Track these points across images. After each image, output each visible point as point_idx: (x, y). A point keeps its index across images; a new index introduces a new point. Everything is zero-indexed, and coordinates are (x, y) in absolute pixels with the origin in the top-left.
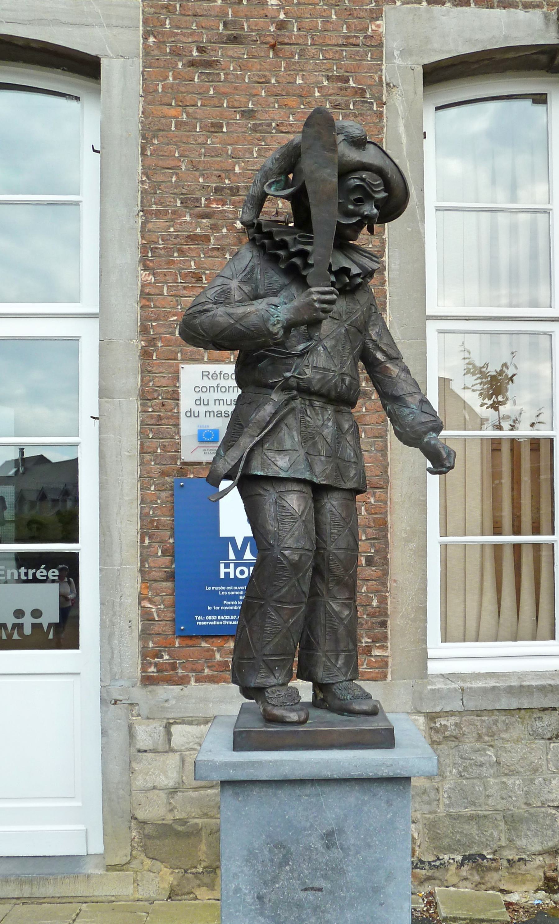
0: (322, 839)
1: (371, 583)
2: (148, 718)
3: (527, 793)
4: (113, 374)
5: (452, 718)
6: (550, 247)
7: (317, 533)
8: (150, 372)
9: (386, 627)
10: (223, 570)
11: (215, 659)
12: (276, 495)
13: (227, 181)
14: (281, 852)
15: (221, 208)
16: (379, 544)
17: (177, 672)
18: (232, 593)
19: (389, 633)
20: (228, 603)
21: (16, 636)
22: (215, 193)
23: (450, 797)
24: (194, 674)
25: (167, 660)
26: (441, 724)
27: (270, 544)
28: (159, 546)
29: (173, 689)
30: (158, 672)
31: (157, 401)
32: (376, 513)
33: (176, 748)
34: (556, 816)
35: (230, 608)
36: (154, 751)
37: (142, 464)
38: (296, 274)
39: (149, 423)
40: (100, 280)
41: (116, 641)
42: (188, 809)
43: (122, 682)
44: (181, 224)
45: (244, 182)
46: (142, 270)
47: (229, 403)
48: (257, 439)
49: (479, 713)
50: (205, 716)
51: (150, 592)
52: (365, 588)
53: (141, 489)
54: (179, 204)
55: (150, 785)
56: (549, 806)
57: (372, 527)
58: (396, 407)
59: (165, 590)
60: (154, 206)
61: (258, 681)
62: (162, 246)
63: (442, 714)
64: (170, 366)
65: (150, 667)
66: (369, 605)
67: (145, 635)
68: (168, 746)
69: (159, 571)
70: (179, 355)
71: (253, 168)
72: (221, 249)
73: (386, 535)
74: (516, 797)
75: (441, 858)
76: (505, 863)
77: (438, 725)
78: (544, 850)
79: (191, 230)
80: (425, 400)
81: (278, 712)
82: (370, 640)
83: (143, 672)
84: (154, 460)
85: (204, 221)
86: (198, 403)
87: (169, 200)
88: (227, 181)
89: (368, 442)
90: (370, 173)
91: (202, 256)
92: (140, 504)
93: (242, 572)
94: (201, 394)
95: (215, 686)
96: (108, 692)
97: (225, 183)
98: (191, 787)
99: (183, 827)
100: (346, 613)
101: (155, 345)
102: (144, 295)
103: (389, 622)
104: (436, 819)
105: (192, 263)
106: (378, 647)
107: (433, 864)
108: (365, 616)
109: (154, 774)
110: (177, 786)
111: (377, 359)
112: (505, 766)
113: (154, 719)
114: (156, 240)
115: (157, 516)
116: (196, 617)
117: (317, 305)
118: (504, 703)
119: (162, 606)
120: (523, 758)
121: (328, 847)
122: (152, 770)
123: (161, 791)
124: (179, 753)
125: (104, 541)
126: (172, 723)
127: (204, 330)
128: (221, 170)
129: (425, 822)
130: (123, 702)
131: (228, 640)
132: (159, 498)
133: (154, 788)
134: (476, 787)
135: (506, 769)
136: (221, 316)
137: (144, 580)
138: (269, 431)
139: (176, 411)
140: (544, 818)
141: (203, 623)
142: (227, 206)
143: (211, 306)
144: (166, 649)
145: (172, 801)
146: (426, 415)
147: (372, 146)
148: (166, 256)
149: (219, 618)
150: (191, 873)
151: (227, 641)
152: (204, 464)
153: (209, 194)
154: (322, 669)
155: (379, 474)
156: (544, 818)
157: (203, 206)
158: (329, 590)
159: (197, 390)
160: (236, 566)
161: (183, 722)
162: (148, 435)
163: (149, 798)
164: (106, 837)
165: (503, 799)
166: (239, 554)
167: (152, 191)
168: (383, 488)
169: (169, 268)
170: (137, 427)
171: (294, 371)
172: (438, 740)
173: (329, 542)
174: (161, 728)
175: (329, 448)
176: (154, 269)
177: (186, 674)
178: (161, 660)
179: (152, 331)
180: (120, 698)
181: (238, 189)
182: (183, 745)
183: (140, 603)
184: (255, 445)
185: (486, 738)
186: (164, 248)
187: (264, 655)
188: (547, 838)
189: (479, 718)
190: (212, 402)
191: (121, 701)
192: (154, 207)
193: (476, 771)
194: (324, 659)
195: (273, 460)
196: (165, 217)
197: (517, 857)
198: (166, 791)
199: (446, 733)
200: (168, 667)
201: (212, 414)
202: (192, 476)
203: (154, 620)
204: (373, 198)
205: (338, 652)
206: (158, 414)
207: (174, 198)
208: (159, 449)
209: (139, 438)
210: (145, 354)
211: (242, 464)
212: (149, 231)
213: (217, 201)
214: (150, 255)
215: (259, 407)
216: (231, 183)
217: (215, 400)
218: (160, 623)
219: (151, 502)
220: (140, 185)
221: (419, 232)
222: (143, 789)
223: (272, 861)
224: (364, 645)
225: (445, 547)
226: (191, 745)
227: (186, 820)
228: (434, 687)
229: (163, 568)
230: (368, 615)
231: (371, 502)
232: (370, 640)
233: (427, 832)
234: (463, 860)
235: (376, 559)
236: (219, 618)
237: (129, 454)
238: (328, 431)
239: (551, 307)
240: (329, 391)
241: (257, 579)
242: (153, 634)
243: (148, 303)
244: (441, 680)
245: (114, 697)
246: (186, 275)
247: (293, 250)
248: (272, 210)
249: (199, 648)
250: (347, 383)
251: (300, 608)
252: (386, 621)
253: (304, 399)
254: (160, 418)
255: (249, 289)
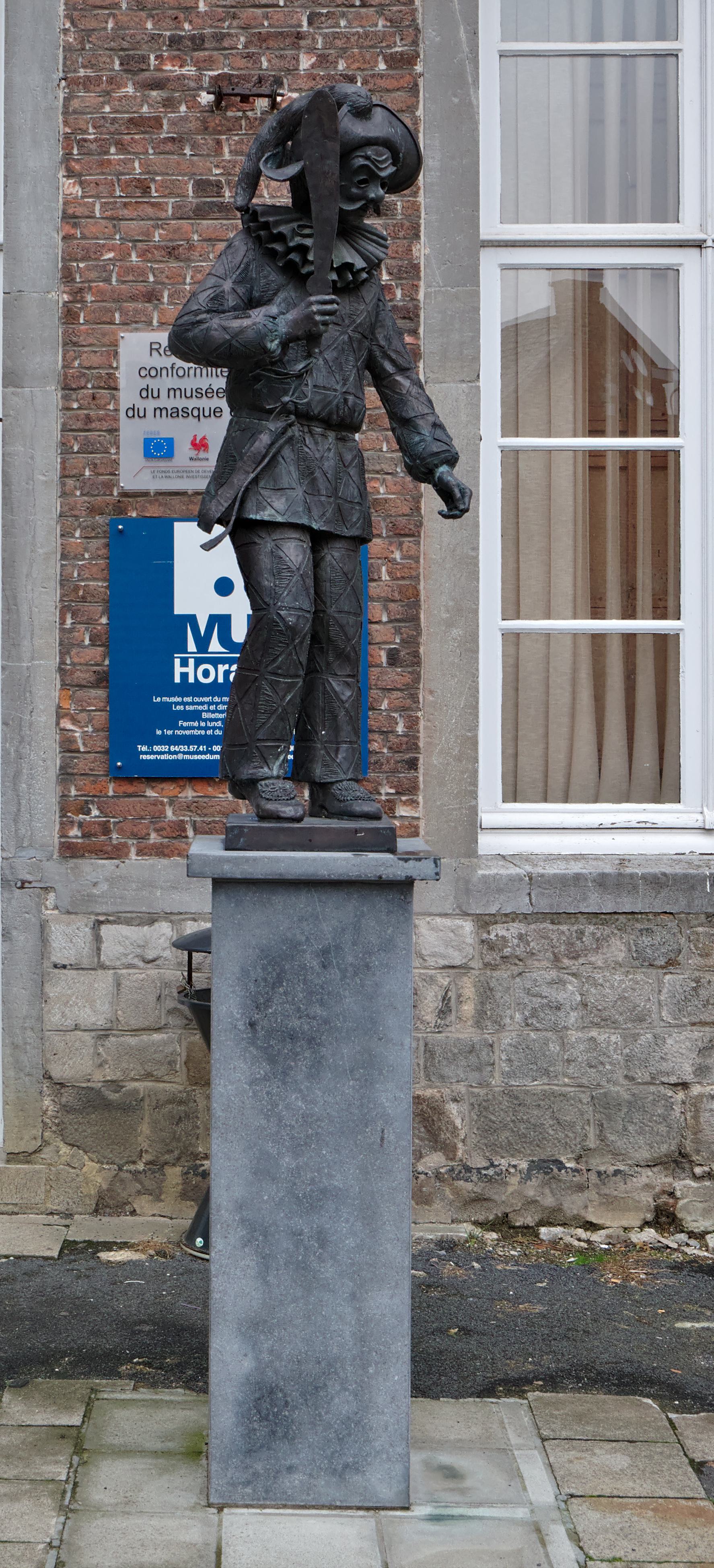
0: (318, 956)
1: (398, 694)
2: (69, 913)
3: (629, 1059)
4: (23, 348)
5: (515, 925)
6: (678, 116)
7: (316, 593)
8: (75, 344)
9: (416, 769)
10: (178, 670)
11: (165, 817)
12: (273, 543)
13: (187, 26)
14: (274, 970)
15: (178, 71)
16: (407, 629)
17: (111, 838)
18: (191, 708)
19: (421, 779)
20: (185, 724)
21: (215, 646)
22: (169, 46)
23: (510, 1060)
24: (135, 842)
25: (96, 817)
26: (497, 935)
27: (265, 603)
28: (87, 629)
29: (104, 866)
30: (84, 836)
31: (85, 391)
32: (403, 578)
33: (108, 963)
34: (673, 1100)
35: (188, 732)
36: (77, 967)
37: (64, 494)
38: (296, 274)
39: (74, 427)
40: (5, 195)
41: (24, 785)
42: (124, 1065)
43: (32, 852)
44: (120, 99)
45: (211, 26)
46: (64, 176)
47: (188, 395)
48: (252, 475)
49: (555, 917)
50: (151, 911)
51: (73, 705)
52: (386, 702)
53: (62, 535)
54: (117, 67)
55: (70, 1023)
56: (664, 1083)
57: (397, 601)
58: (405, 432)
59: (94, 702)
60: (82, 70)
61: (250, 772)
62: (93, 137)
63: (498, 918)
64: (104, 335)
65: (72, 828)
66: (392, 732)
67: (66, 775)
68: (96, 960)
69: (87, 671)
70: (117, 315)
71: (224, 3)
72: (177, 141)
73: (418, 613)
74: (610, 1063)
75: (496, 1163)
76: (593, 1177)
77: (492, 936)
78: (654, 1160)
79: (134, 109)
80: (438, 423)
81: (270, 806)
82: (392, 791)
83: (61, 837)
84: (81, 488)
85: (154, 93)
86: (144, 394)
87: (104, 59)
88: (187, 26)
89: (392, 458)
90: (375, 147)
91: (151, 151)
92: (61, 560)
93: (206, 674)
94: (148, 380)
95: (165, 861)
96: (12, 868)
97: (184, 30)
98: (129, 1028)
99: (117, 1095)
100: (348, 693)
101: (83, 301)
102: (69, 218)
103: (421, 761)
104: (490, 1097)
105: (137, 164)
106: (405, 803)
107: (484, 1172)
108: (385, 750)
109: (77, 1004)
110: (108, 1025)
111: (385, 370)
112: (594, 1010)
113: (76, 913)
114: (84, 128)
115: (83, 580)
116: (139, 746)
117: (318, 318)
118: (595, 902)
119: (90, 729)
120: (622, 998)
121: (324, 967)
122: (74, 999)
123: (86, 1034)
124: (112, 971)
125: (9, 621)
126: (102, 922)
127: (197, 346)
128: (178, 8)
129: (473, 1100)
130: (33, 885)
131: (184, 786)
132: (86, 550)
133: (77, 1028)
134: (551, 1045)
135: (596, 1016)
136: (216, 330)
137: (64, 685)
138: (264, 468)
139: (111, 407)
140: (654, 1102)
141: (149, 757)
142: (187, 68)
143: (204, 316)
144: (96, 799)
145: (101, 1050)
146: (439, 443)
147: (379, 109)
148: (99, 154)
149: (172, 748)
150: (127, 1171)
151: (183, 788)
152: (152, 494)
153: (160, 49)
154: (320, 765)
155: (408, 511)
156: (654, 1102)
157: (152, 68)
158: (328, 664)
159: (143, 373)
160: (198, 662)
161: (118, 919)
162: (72, 447)
163: (70, 1045)
164: (7, 1107)
165: (591, 1067)
166: (203, 643)
167: (79, 47)
168: (413, 536)
169: (103, 173)
170: (56, 435)
171: (293, 394)
172: (493, 962)
173: (328, 604)
174: (87, 929)
175: (329, 486)
176: (80, 175)
177: (123, 841)
178: (87, 818)
179: (78, 276)
180: (29, 877)
181: (202, 38)
182: (118, 959)
183: (58, 724)
184: (250, 483)
185: (566, 962)
186: (96, 140)
187: (258, 740)
188: (658, 1138)
189: (555, 927)
190: (163, 394)
191: (30, 883)
192: (82, 72)
193: (550, 1017)
194: (322, 752)
195: (269, 500)
196: (98, 89)
197: (612, 1169)
198: (93, 1034)
199: (505, 950)
200: (98, 829)
201: (164, 412)
202: (134, 515)
203: (78, 751)
204: (379, 177)
205: (338, 743)
206: (85, 412)
207: (110, 57)
208: (87, 470)
209: (59, 451)
210: (69, 315)
211: (237, 506)
212: (75, 112)
213: (172, 59)
214: (75, 152)
215: (254, 437)
216: (194, 29)
217: (169, 390)
218: (87, 756)
219: (75, 557)
220: (62, 37)
221: (470, 104)
222: (61, 1028)
223: (265, 980)
224: (383, 798)
225: (512, 639)
226: (130, 959)
227: (121, 1084)
228: (487, 872)
229: (92, 665)
230: (390, 748)
231: (395, 559)
232: (392, 791)
233: (475, 1117)
234: (530, 1170)
235: (402, 653)
236: (172, 748)
237: (44, 478)
238: (329, 464)
239: (678, 222)
240: (330, 414)
241: (251, 646)
242: (76, 774)
243: (73, 232)
244: (500, 863)
245: (21, 877)
246: (128, 184)
247: (291, 244)
248: (253, 72)
249: (143, 799)
250: (350, 403)
251: (298, 682)
252: (417, 759)
253: (302, 425)
254: (88, 419)
255: (244, 290)
